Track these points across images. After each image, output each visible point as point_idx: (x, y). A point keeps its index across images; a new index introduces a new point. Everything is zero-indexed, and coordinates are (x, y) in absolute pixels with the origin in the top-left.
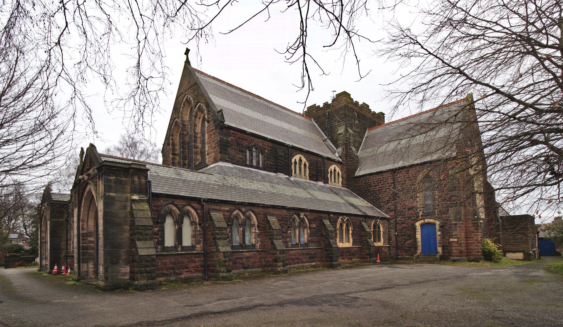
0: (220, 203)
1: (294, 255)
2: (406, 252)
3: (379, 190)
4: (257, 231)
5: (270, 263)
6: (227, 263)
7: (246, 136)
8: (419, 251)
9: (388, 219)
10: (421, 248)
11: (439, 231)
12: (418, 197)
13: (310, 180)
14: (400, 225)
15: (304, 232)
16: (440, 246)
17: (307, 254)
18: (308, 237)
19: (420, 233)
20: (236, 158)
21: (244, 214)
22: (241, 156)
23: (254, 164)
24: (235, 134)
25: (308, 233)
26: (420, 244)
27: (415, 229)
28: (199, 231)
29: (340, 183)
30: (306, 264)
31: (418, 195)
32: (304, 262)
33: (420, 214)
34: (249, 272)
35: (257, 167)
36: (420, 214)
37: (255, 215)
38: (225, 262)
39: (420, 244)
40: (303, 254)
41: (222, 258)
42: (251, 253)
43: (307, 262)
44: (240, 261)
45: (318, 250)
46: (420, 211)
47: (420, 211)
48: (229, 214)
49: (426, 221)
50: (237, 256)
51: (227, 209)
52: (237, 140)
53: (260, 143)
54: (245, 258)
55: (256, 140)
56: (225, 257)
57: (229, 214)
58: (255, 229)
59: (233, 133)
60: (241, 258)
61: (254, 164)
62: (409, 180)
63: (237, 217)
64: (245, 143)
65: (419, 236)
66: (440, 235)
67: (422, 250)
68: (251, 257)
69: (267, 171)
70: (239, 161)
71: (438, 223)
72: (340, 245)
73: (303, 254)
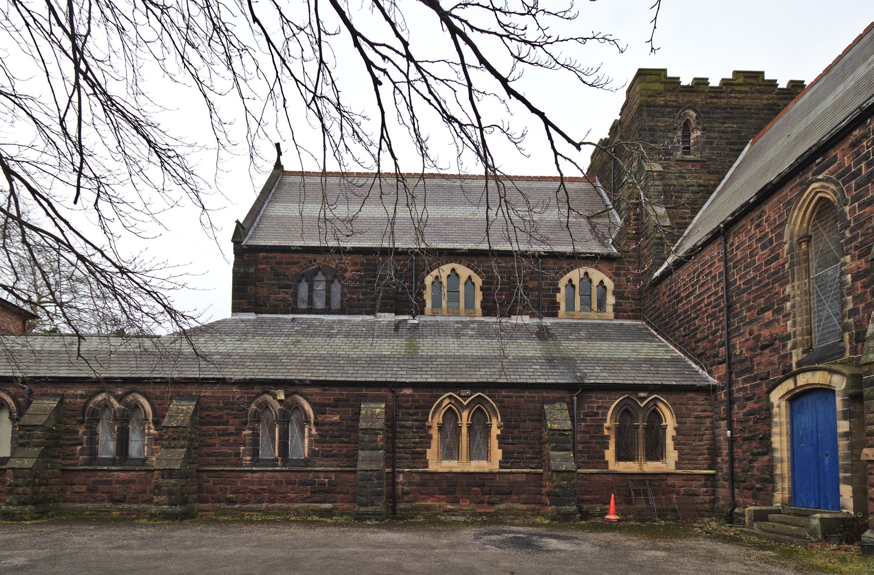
0: (67, 382)
1: (260, 482)
2: (754, 497)
3: (695, 306)
4: (152, 431)
5: (198, 493)
6: (20, 489)
7: (296, 256)
8: (780, 497)
9: (708, 390)
10: (787, 484)
11: (846, 416)
12: (786, 299)
13: (484, 315)
14: (740, 408)
15: (302, 431)
16: (847, 481)
17: (303, 483)
18: (310, 445)
19: (785, 428)
20: (272, 300)
21: (120, 399)
22: (281, 296)
23: (320, 304)
24: (271, 258)
25: (310, 435)
26: (783, 468)
27: (766, 414)
28: (315, 436)
29: (610, 309)
30: (297, 505)
31: (788, 289)
32: (292, 501)
33: (794, 360)
34: (119, 510)
35: (328, 311)
36: (794, 360)
37: (307, 399)
38: (17, 486)
39: (783, 468)
40: (289, 483)
41: (9, 480)
42: (131, 473)
43: (303, 501)
44: (106, 488)
45: (345, 476)
46: (794, 347)
47: (794, 347)
48: (84, 401)
49: (803, 379)
50: (97, 478)
51: (79, 392)
52: (272, 269)
53: (333, 262)
54: (117, 482)
55: (320, 259)
56: (16, 477)
57: (84, 401)
58: (149, 428)
59: (264, 258)
60: (109, 483)
61: (320, 304)
62: (764, 247)
63: (106, 405)
64: (295, 269)
65: (780, 442)
66: (846, 435)
67: (793, 490)
68: (131, 482)
69: (349, 314)
70: (277, 306)
71: (839, 383)
72: (437, 463)
73: (292, 483)
